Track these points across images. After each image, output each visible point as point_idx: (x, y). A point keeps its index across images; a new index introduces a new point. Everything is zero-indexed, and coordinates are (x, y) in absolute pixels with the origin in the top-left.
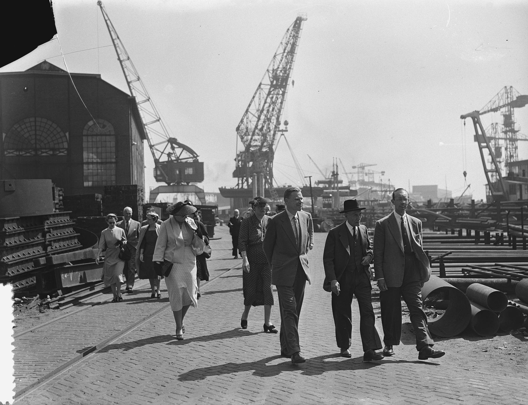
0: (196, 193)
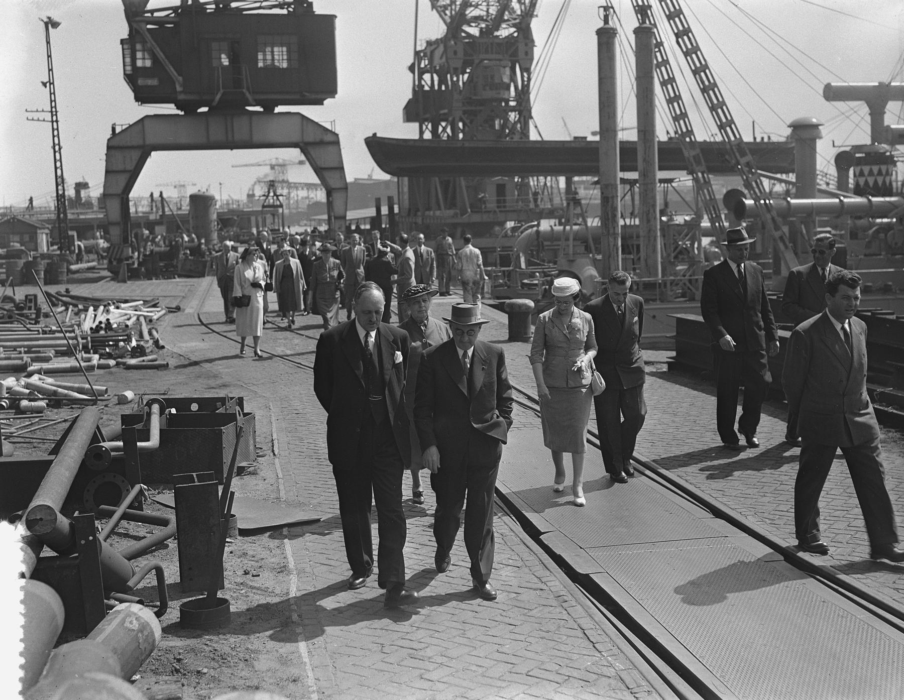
0: (304, 147)
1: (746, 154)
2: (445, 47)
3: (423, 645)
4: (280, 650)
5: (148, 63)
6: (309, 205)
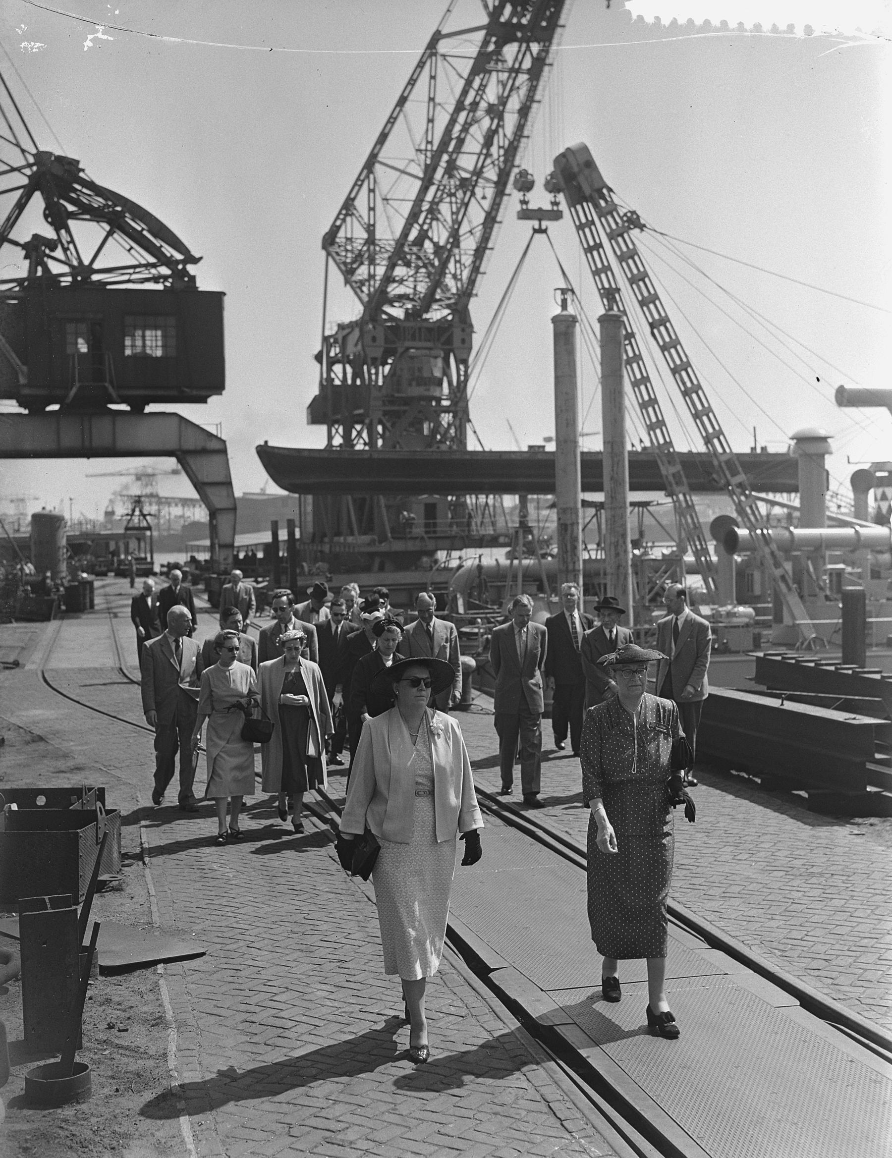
0: (183, 456)
1: (738, 473)
2: (361, 331)
3: (344, 1125)
4: (158, 1134)
6: (184, 526)
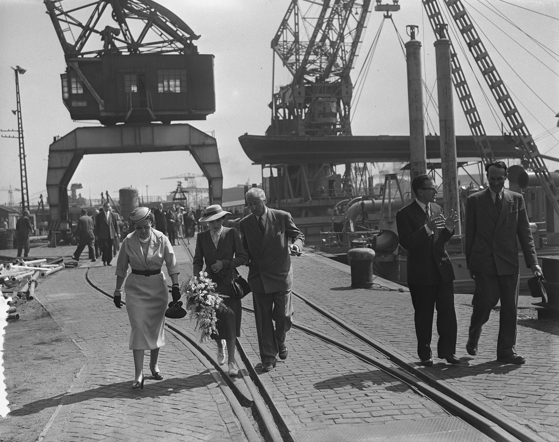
2: (292, 90)
5: (81, 91)
